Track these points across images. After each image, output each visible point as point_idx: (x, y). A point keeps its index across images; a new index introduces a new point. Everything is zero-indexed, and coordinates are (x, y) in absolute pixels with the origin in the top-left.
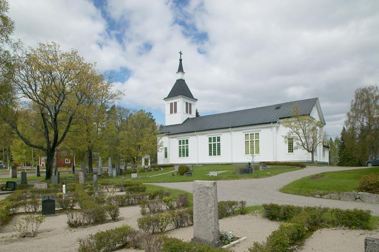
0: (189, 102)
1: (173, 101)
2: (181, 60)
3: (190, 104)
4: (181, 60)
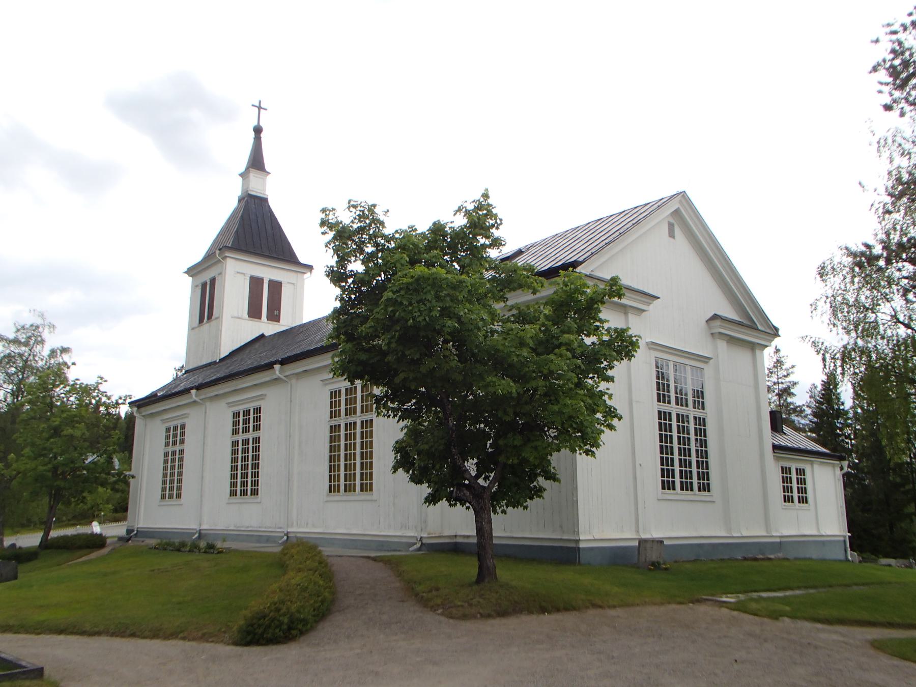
0: (268, 272)
1: (206, 277)
2: (258, 130)
3: (276, 287)
4: (258, 130)
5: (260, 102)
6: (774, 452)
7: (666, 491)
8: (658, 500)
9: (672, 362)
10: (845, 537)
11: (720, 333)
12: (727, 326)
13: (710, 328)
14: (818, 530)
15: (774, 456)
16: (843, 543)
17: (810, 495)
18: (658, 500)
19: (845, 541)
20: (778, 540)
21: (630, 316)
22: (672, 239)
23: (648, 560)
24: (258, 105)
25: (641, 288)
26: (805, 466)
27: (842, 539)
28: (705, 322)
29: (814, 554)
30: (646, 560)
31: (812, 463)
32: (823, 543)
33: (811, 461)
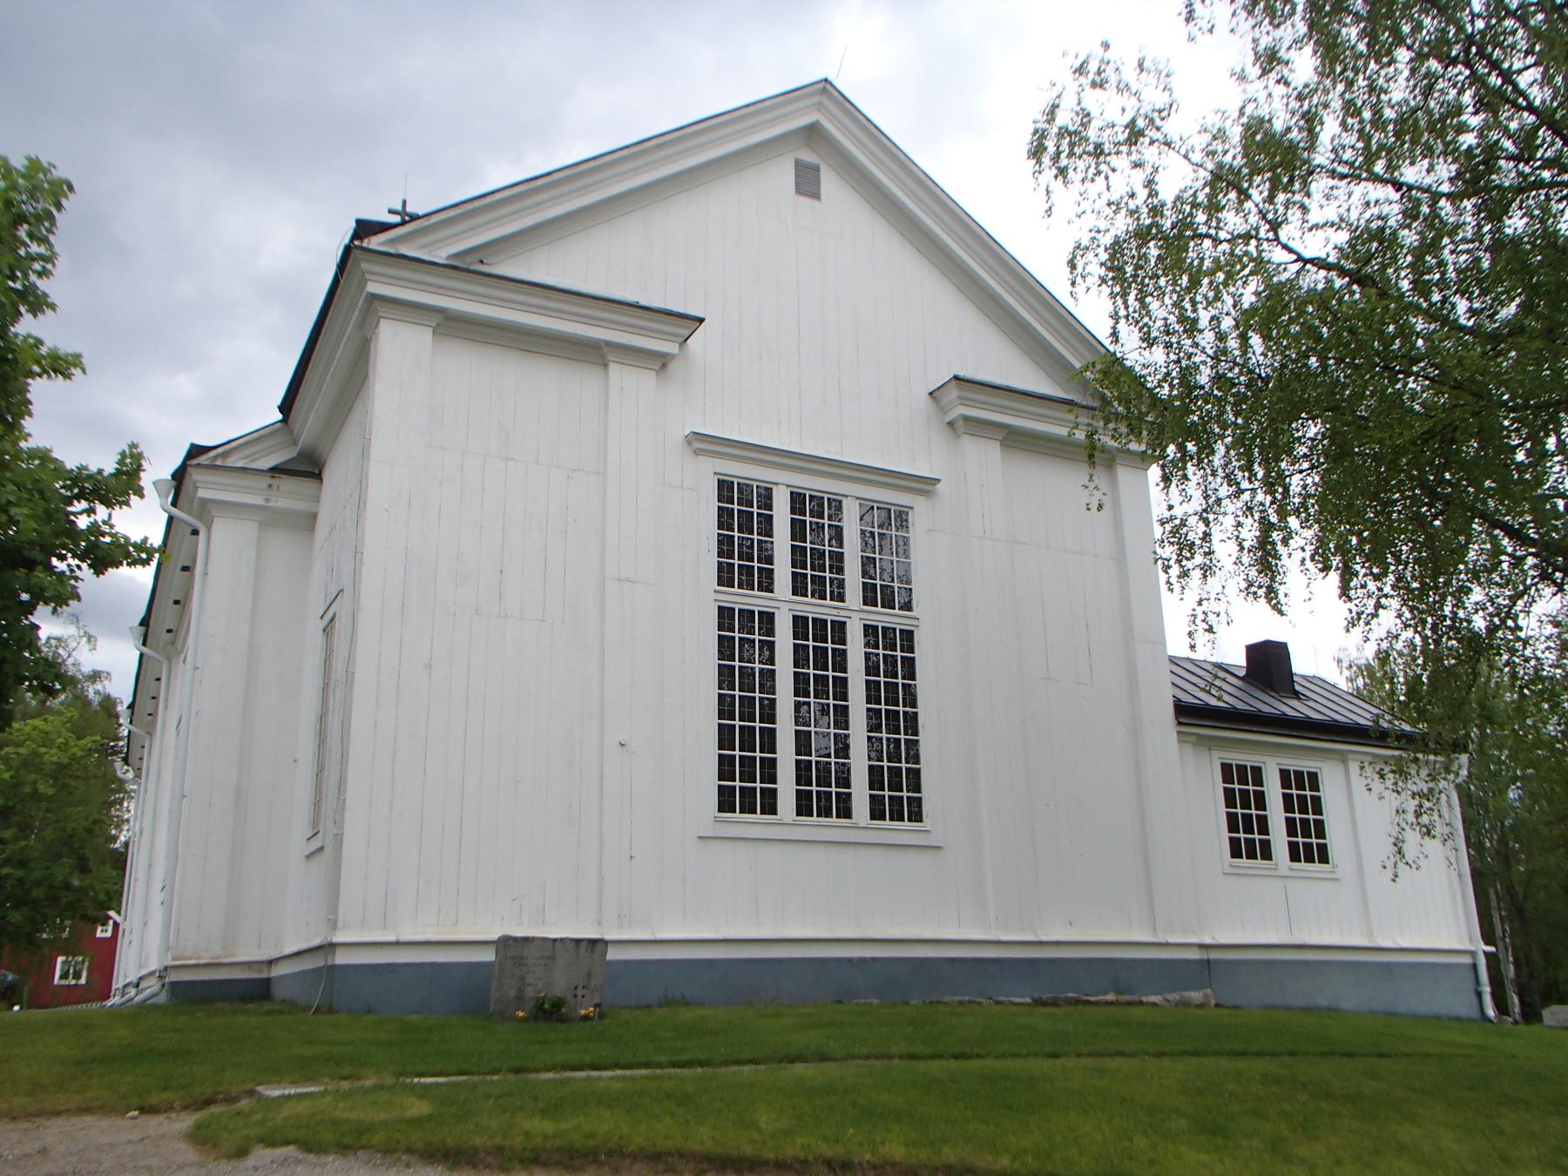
5: (404, 203)
6: (1179, 723)
7: (1244, 861)
8: (1225, 874)
9: (783, 488)
10: (1473, 954)
11: (966, 419)
12: (984, 398)
13: (943, 411)
14: (1371, 934)
15: (1179, 733)
16: (1470, 974)
17: (1336, 838)
18: (1225, 874)
19: (1475, 967)
20: (1194, 955)
21: (614, 369)
22: (806, 201)
23: (529, 992)
24: (399, 208)
25: (682, 310)
26: (1262, 758)
27: (1467, 960)
28: (924, 394)
29: (1350, 997)
30: (520, 991)
31: (1343, 758)
32: (1388, 967)
33: (1341, 752)
